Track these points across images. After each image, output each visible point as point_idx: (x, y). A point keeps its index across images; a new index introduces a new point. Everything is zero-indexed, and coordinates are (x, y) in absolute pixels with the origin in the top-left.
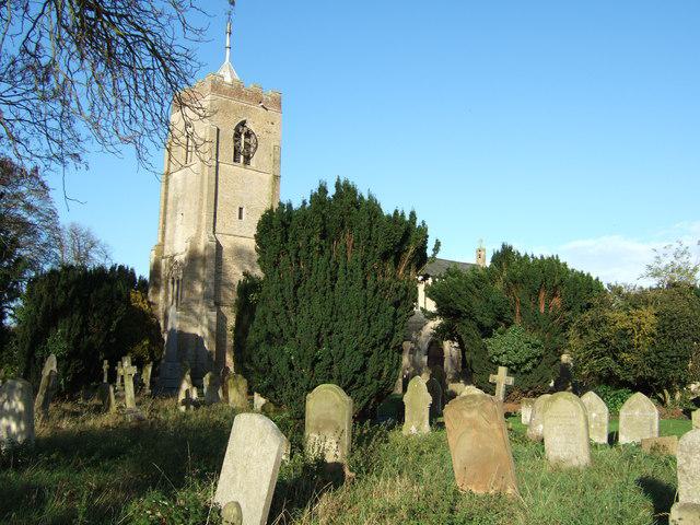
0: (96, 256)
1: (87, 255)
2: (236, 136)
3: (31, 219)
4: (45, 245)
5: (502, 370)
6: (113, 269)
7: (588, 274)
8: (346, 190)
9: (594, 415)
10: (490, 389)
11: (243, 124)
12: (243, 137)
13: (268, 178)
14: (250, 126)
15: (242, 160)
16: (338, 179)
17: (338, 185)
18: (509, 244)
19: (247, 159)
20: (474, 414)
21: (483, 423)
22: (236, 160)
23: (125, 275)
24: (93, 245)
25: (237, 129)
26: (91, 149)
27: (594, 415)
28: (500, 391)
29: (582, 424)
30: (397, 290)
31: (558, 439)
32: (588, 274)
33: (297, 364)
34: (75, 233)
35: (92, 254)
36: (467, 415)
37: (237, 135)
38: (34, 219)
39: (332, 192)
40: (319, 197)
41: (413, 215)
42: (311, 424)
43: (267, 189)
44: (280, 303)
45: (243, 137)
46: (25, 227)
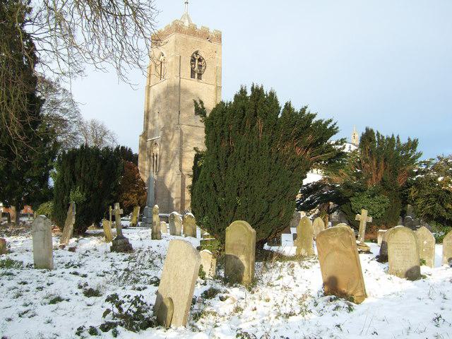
0: (107, 141)
1: (101, 139)
2: (192, 61)
3: (65, 117)
4: (75, 134)
5: (364, 212)
6: (117, 148)
7: (272, 94)
8: (258, 92)
9: (425, 242)
10: (355, 225)
11: (196, 53)
12: (197, 61)
13: (213, 88)
14: (202, 54)
15: (196, 77)
16: (306, 107)
17: (252, 88)
18: (370, 127)
19: (200, 75)
20: (336, 241)
21: (342, 247)
22: (193, 76)
23: (124, 153)
24: (105, 134)
25: (193, 57)
26: (88, 67)
27: (425, 242)
28: (363, 227)
29: (415, 249)
30: (293, 160)
31: (397, 259)
32: (272, 94)
33: (224, 208)
34: (94, 126)
35: (104, 139)
36: (331, 242)
37: (193, 60)
38: (67, 117)
39: (249, 93)
40: (241, 96)
41: (262, 86)
42: (229, 247)
43: (213, 95)
44: (215, 166)
45: (197, 61)
46: (62, 122)
